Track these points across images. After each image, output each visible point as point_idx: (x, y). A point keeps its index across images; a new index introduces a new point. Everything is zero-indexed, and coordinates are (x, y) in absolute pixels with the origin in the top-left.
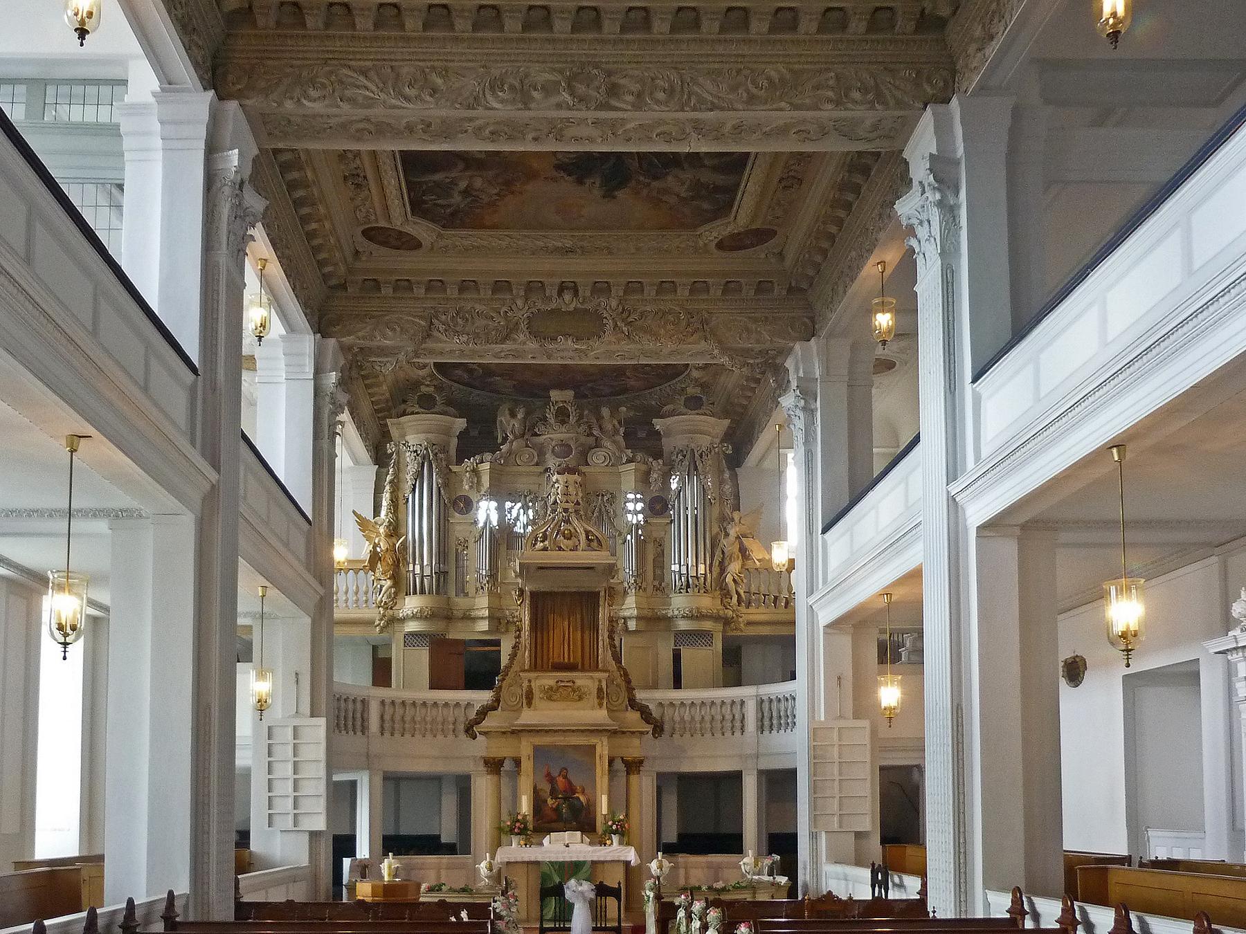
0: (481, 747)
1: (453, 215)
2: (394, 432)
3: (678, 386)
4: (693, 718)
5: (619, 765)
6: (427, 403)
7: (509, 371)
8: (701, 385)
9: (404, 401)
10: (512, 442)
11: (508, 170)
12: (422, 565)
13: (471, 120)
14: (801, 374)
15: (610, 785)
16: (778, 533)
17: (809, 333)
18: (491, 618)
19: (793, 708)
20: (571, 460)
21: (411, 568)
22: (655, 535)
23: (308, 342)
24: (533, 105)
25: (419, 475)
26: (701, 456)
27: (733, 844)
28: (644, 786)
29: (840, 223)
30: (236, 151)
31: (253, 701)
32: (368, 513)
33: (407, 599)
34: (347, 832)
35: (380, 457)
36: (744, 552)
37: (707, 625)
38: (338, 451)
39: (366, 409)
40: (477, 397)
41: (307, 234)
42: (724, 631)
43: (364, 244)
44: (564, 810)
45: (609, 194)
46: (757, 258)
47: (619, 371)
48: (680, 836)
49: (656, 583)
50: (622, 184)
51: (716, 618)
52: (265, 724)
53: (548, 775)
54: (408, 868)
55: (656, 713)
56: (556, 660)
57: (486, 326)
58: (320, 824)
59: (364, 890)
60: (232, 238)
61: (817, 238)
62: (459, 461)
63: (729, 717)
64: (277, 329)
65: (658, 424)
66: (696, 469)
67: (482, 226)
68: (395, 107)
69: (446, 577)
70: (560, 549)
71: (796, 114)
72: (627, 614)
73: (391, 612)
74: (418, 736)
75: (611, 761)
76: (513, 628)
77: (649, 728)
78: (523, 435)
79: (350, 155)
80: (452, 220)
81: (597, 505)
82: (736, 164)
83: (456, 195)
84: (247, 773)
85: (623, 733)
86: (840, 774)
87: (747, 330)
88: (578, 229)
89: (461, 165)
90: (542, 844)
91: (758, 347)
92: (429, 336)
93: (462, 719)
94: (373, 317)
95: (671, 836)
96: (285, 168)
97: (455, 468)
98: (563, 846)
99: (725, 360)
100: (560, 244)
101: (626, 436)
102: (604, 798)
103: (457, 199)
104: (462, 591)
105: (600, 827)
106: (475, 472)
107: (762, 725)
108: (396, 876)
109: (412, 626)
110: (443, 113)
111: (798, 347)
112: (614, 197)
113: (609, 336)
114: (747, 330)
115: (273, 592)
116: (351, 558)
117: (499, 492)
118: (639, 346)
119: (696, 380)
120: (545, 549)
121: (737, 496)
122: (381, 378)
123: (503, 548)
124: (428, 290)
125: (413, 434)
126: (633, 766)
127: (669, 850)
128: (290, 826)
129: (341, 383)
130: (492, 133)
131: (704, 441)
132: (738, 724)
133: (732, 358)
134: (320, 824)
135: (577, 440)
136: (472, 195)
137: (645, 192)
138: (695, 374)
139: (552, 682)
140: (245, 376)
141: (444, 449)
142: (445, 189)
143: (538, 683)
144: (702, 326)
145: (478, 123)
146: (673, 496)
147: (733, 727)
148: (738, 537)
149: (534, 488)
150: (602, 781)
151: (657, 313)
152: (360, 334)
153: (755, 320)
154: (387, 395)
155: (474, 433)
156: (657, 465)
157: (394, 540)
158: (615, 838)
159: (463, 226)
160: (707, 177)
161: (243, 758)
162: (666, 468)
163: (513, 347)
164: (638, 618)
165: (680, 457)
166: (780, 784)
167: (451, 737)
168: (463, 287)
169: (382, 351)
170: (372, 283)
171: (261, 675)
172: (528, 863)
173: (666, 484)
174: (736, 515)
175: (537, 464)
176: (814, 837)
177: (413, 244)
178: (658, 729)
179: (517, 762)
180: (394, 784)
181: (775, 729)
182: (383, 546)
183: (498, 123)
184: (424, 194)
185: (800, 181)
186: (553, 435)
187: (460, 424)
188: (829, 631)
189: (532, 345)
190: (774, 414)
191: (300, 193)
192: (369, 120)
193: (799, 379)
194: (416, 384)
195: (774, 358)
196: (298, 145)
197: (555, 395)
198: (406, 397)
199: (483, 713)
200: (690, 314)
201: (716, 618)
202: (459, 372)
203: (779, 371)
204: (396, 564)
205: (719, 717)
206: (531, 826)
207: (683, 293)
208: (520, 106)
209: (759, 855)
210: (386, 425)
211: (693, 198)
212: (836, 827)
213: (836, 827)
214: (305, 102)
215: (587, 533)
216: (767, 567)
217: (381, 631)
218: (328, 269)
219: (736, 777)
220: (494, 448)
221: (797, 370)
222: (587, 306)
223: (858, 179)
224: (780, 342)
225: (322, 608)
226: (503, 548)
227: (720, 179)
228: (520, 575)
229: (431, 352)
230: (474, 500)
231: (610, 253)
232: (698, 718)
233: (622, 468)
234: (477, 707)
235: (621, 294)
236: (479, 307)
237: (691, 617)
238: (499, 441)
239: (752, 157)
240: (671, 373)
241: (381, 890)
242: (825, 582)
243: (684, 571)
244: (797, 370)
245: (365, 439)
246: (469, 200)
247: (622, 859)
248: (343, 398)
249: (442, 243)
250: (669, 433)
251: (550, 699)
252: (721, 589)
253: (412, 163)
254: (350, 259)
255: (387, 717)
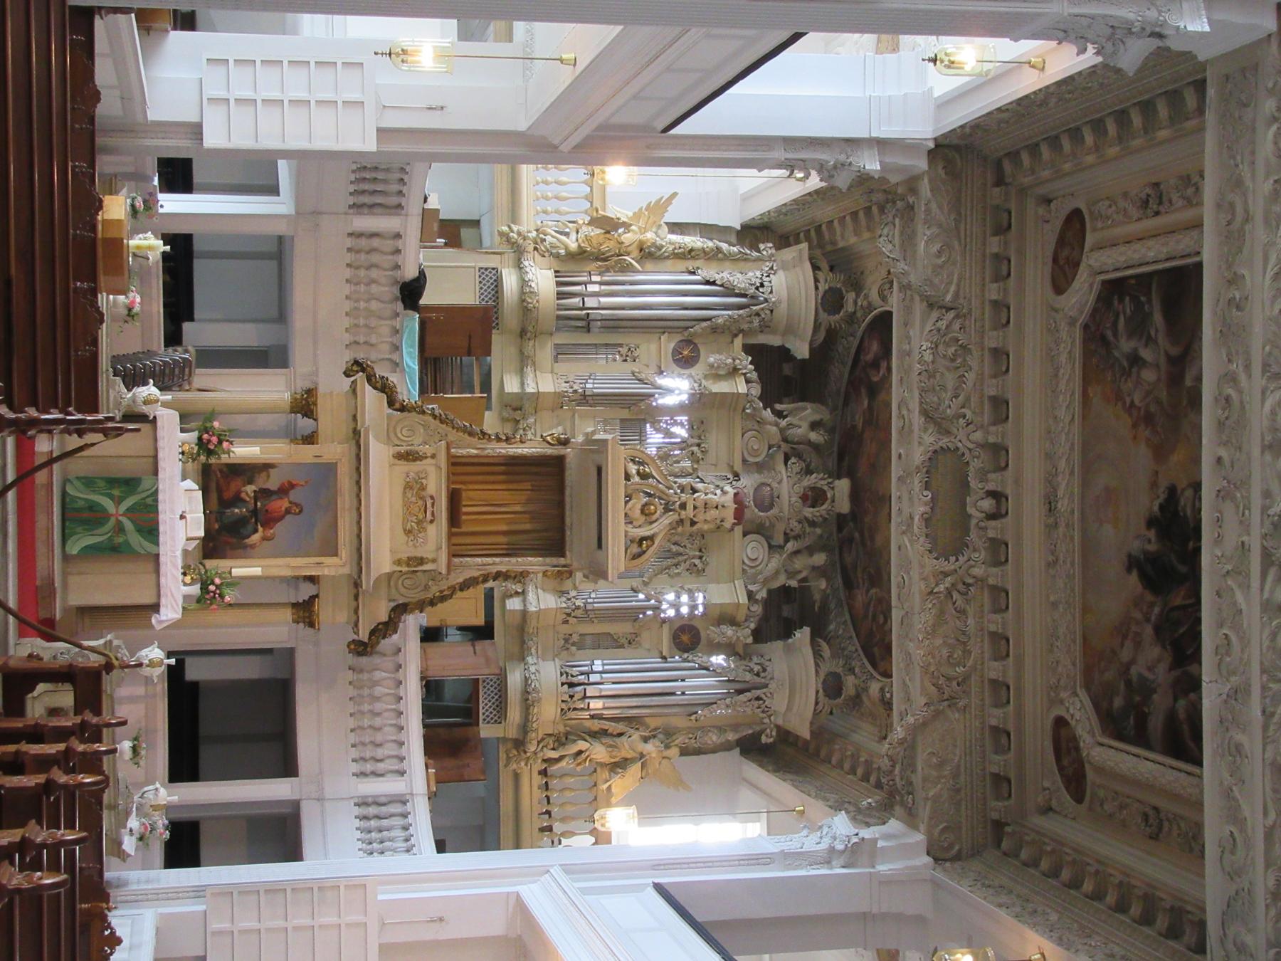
0: (332, 385)
1: (1103, 338)
2: (789, 254)
3: (856, 664)
4: (378, 699)
5: (306, 591)
6: (831, 301)
7: (878, 422)
8: (858, 696)
9: (832, 269)
10: (777, 425)
11: (1172, 412)
12: (598, 293)
13: (1247, 367)
14: (880, 844)
15: (273, 578)
16: (649, 811)
17: (939, 854)
18: (522, 396)
19: (395, 850)
20: (752, 512)
21: (595, 278)
22: (645, 635)
23: (924, 129)
24: (1268, 457)
25: (729, 291)
26: (758, 699)
27: (184, 767)
28: (276, 630)
29: (1098, 896)
30: (1207, 29)
31: (404, 41)
32: (673, 215)
33: (550, 274)
34: (197, 178)
35: (754, 233)
36: (618, 766)
37: (514, 714)
38: (766, 172)
39: (824, 213)
40: (839, 373)
41: (1078, 129)
42: (505, 740)
43: (1061, 210)
44: (239, 509)
45: (1133, 563)
46: (1041, 773)
47: (879, 577)
48: (195, 685)
49: (575, 638)
50: (1144, 576)
51: (525, 727)
52: (366, 58)
53: (292, 486)
54: (144, 275)
55: (386, 644)
56: (464, 494)
57: (943, 388)
58: (212, 139)
59: (115, 208)
60: (1085, 22)
61: (1074, 862)
62: (748, 349)
63: (380, 753)
64: (942, 84)
65: (802, 635)
66: (740, 692)
67: (1086, 381)
68: (1266, 259)
69: (583, 329)
70: (629, 497)
71: (1260, 835)
72: (531, 596)
73: (531, 248)
74: (347, 289)
75: (312, 579)
76: (508, 429)
77: (364, 635)
78: (785, 440)
79: (1190, 191)
80: (1096, 337)
81: (688, 550)
82: (1183, 743)
83: (1133, 344)
84: (295, 31)
85: (356, 598)
86: (296, 929)
87: (941, 765)
88: (1083, 518)
89: (1175, 351)
90: (184, 479)
91: (917, 779)
92: (931, 306)
93: (373, 356)
94: (957, 228)
95: (195, 671)
96: (1174, 97)
97: (738, 342)
98: (182, 512)
99: (899, 732)
100: (1060, 494)
101: (785, 590)
102: (257, 571)
103: (1126, 345)
104: (561, 352)
105: (211, 564)
106: (734, 372)
107: (366, 804)
108: (135, 255)
109: (510, 281)
110: (1257, 329)
111: (919, 838)
112: (1129, 570)
113: (931, 564)
114: (941, 765)
115: (566, 76)
116: (608, 189)
117: (701, 405)
118: (917, 609)
119: (866, 690)
120: (628, 477)
121: (698, 752)
122: (866, 235)
123: (625, 414)
124: (995, 304)
125: (787, 282)
126: (305, 612)
127: (175, 674)
128: (209, 92)
129: (863, 179)
130: (1228, 399)
131: (778, 703)
132: (369, 767)
133: (902, 742)
134: (212, 139)
135: (778, 519)
136: (1131, 366)
137: (1138, 615)
138: (874, 688)
139: (431, 488)
140: (869, 39)
141: (765, 327)
142: (1139, 327)
143: (432, 471)
144: (947, 695)
145: (1243, 378)
146: (700, 658)
147: (363, 759)
148: (642, 756)
149: (711, 457)
150: (284, 566)
151: (964, 633)
152: (934, 206)
153: (956, 776)
154: (841, 244)
155: (787, 369)
156: (745, 635)
157: (636, 253)
158: (195, 590)
159: (1087, 355)
160: (1160, 703)
161: (313, 25)
162: (740, 650)
163: (916, 428)
164: (524, 613)
165: (756, 668)
166: (279, 836)
167: (347, 338)
168: (999, 354)
169: (908, 240)
170: (1005, 224)
171: (442, 55)
172: (156, 457)
173: (715, 648)
174: (674, 752)
175: (744, 461)
176: (198, 892)
177: (1061, 279)
178: (361, 648)
179: (310, 439)
180: (275, 253)
181: (364, 824)
182: (628, 238)
183: (1243, 408)
184: (1135, 299)
185: (1154, 837)
186: (787, 484)
187: (801, 350)
188: (512, 901)
189: (918, 456)
190: (820, 804)
191: (1137, 119)
192: (1247, 220)
193: (875, 841)
194: (857, 285)
195: (903, 804)
196: (1210, 117)
197: (843, 485)
198: (837, 266)
199: (385, 388)
200: (964, 681)
201: (525, 727)
202: (875, 347)
203: (883, 811)
204: (600, 257)
205: (379, 738)
206: (213, 460)
207: (994, 670)
208: (1268, 438)
209: (168, 808)
210: (798, 242)
211: (1128, 683)
212: (214, 925)
213: (214, 925)
214: (1274, 128)
215: (651, 538)
216: (597, 801)
217: (501, 234)
218: (1025, 157)
219: (288, 768)
220: (768, 398)
221: (887, 837)
222: (973, 535)
223: (1162, 922)
224: (925, 812)
225: (539, 147)
226: (625, 414)
227: (1156, 723)
228: (589, 440)
229: (908, 310)
230: (693, 371)
231: (1049, 565)
232: (379, 706)
233: (739, 583)
234: (393, 378)
235: (991, 581)
236: (971, 377)
237: (526, 692)
238: (778, 407)
239: (1195, 770)
240: (877, 650)
241: (115, 235)
242: (584, 891)
243: (593, 678)
244: (887, 837)
245: (778, 210)
246: (1125, 364)
247: (163, 601)
248: (842, 181)
249: (1063, 326)
250: (789, 650)
251: (408, 487)
252: (567, 734)
253: (1178, 288)
254: (1042, 191)
255: (376, 242)
